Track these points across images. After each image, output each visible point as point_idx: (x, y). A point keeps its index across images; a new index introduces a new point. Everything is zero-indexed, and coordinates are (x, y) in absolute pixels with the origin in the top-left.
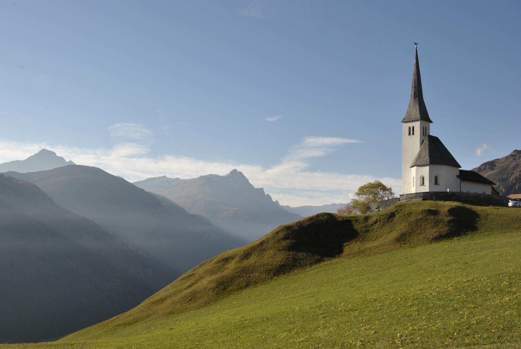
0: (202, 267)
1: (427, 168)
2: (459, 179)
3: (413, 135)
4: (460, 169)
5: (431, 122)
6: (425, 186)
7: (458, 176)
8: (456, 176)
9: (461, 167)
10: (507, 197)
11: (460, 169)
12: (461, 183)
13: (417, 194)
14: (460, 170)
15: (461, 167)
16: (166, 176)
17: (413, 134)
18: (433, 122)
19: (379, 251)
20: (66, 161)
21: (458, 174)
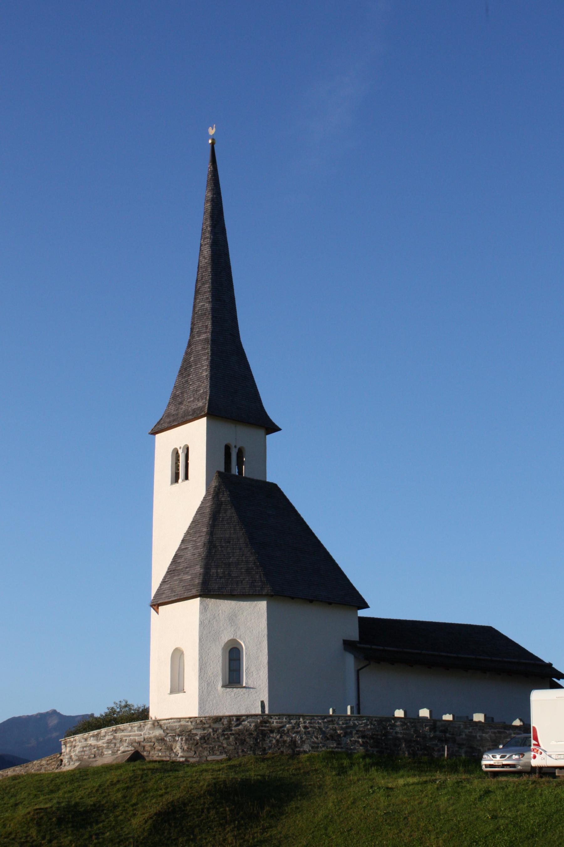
0: (146, 736)
1: (201, 424)
2: (350, 660)
3: (187, 482)
4: (362, 613)
5: (272, 428)
6: (185, 692)
7: (348, 645)
8: (342, 642)
9: (365, 605)
10: (429, 718)
11: (362, 613)
12: (360, 672)
13: (192, 719)
14: (361, 619)
15: (365, 605)
16: (58, 711)
17: (186, 478)
18: (280, 427)
19: (86, 839)
20: (445, 714)
21: (354, 635)
